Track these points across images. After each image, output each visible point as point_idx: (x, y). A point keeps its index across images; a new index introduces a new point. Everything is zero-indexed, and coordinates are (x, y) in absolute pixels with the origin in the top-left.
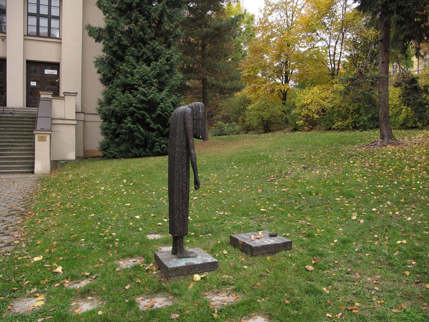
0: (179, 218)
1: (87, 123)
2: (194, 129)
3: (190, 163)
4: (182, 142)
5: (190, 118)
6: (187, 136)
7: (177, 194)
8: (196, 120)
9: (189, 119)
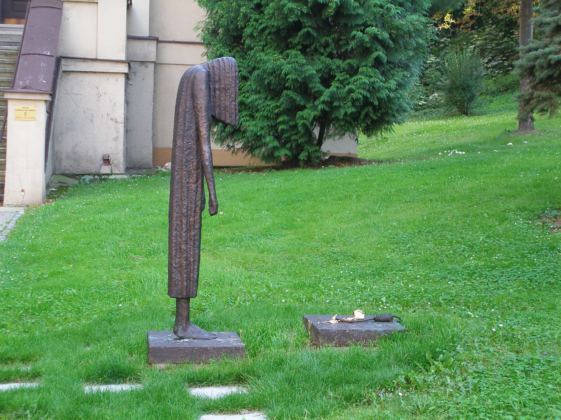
0: (181, 266)
1: (159, 66)
4: (188, 130)
7: (179, 223)
8: (220, 90)
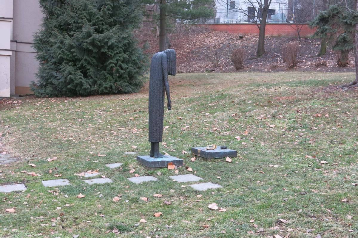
2: (169, 68)
3: (165, 92)
5: (166, 60)
6: (163, 73)
9: (165, 61)
